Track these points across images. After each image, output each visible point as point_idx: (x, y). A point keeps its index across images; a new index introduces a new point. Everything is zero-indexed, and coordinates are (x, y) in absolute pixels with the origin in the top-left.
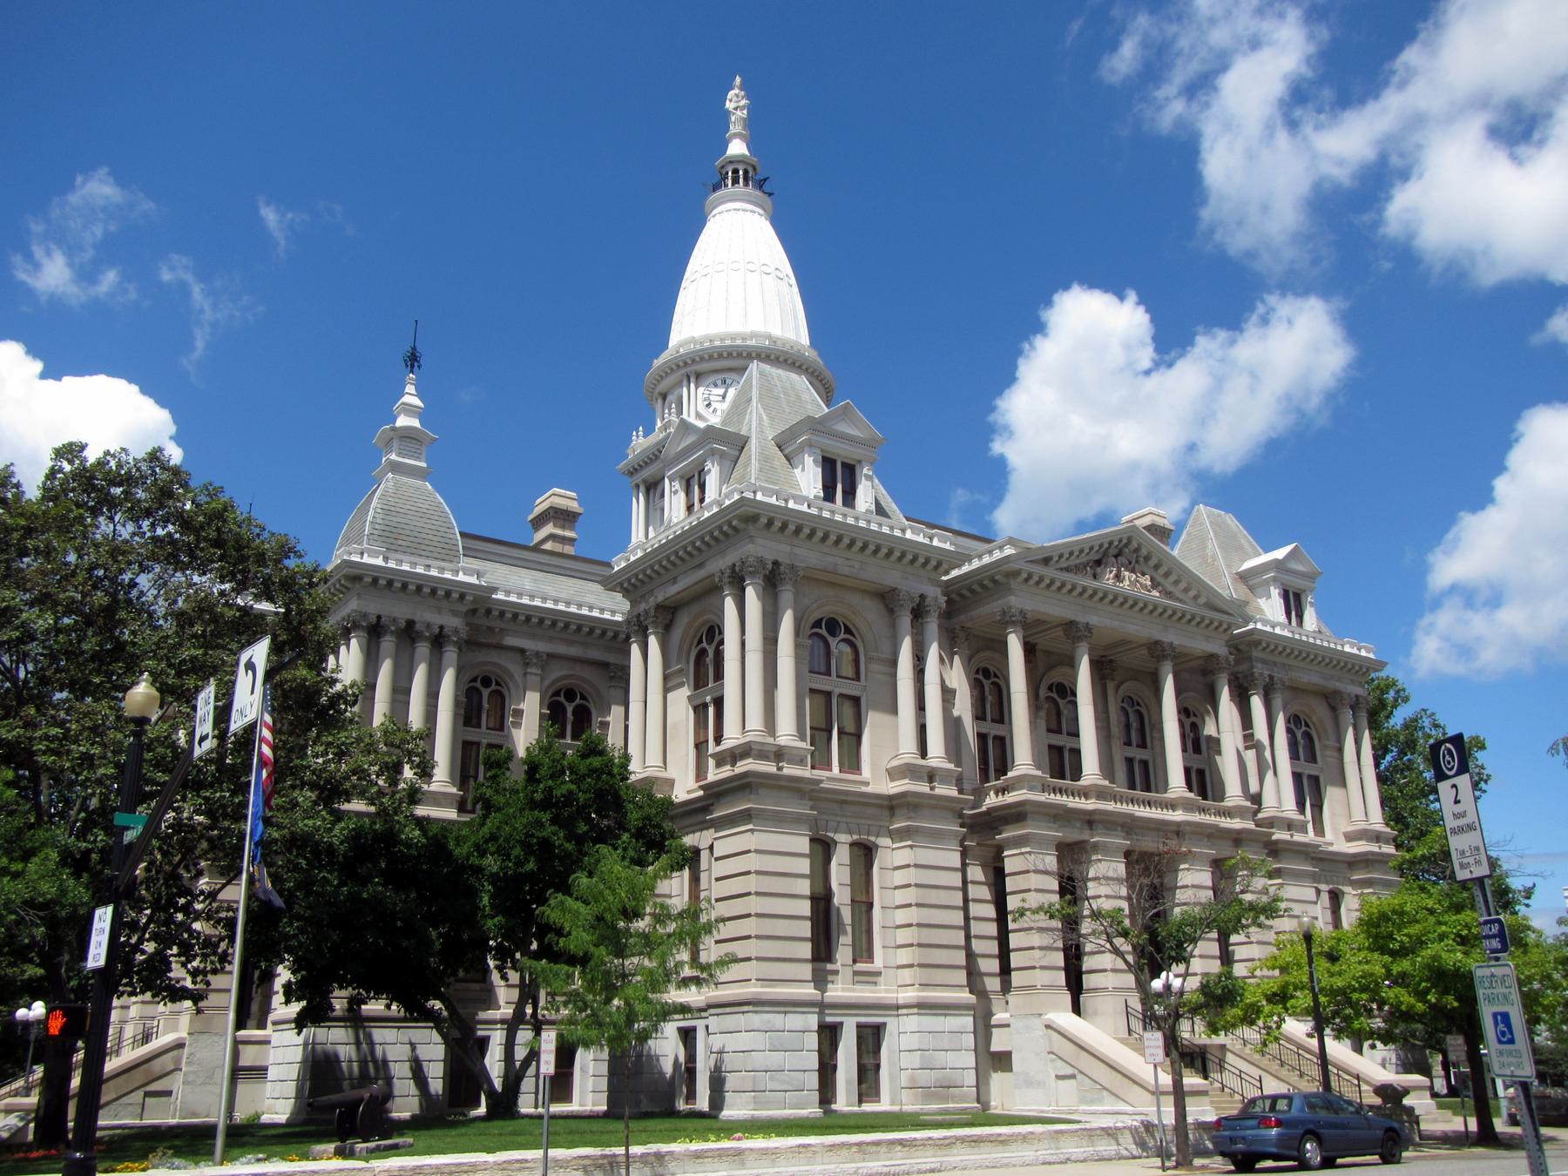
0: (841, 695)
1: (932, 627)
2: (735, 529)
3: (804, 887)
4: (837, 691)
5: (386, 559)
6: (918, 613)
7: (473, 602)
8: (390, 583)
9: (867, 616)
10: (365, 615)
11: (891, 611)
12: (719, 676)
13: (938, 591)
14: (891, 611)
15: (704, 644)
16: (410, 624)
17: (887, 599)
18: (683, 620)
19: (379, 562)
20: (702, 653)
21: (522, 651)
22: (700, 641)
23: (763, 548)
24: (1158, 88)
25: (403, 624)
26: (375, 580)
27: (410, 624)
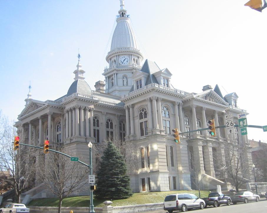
0: (167, 120)
6: (179, 106)
10: (78, 106)
20: (141, 113)
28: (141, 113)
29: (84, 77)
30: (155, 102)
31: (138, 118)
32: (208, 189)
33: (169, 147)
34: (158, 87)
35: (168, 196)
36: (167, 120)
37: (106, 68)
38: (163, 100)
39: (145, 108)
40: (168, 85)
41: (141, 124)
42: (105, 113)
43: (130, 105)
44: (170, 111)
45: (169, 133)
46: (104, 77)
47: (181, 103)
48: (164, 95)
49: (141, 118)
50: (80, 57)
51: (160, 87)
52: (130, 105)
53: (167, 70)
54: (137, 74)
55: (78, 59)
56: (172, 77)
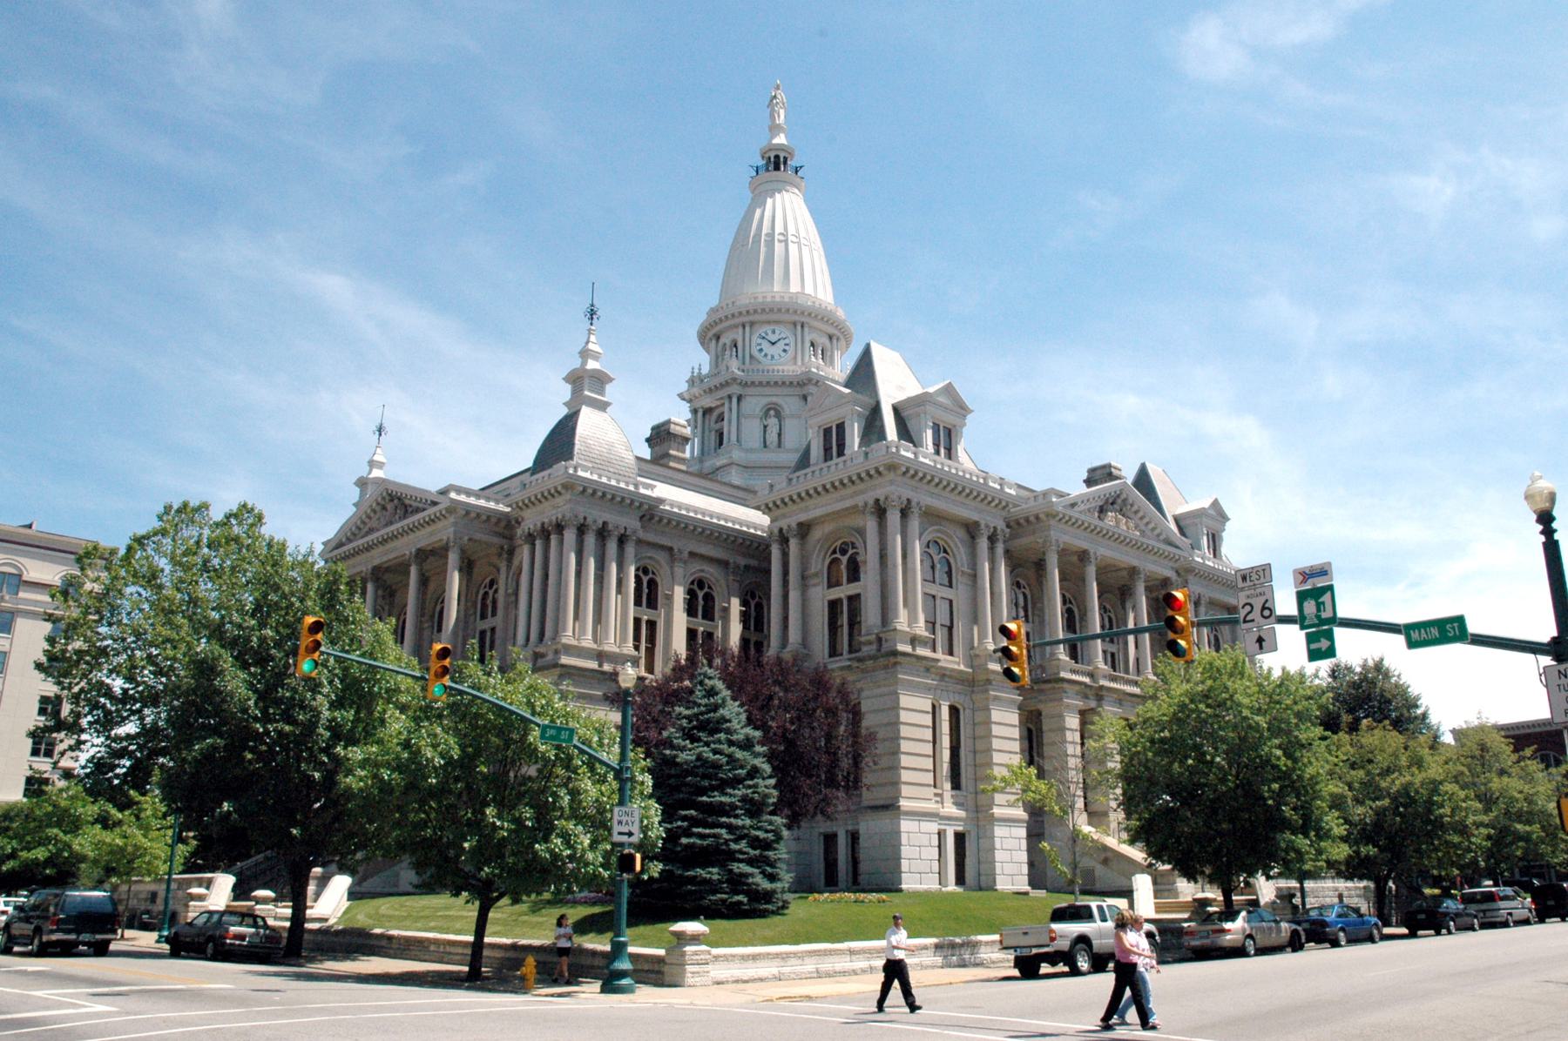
6: (992, 539)
11: (973, 537)
17: (971, 530)
21: (671, 549)
40: (950, 454)
42: (686, 555)
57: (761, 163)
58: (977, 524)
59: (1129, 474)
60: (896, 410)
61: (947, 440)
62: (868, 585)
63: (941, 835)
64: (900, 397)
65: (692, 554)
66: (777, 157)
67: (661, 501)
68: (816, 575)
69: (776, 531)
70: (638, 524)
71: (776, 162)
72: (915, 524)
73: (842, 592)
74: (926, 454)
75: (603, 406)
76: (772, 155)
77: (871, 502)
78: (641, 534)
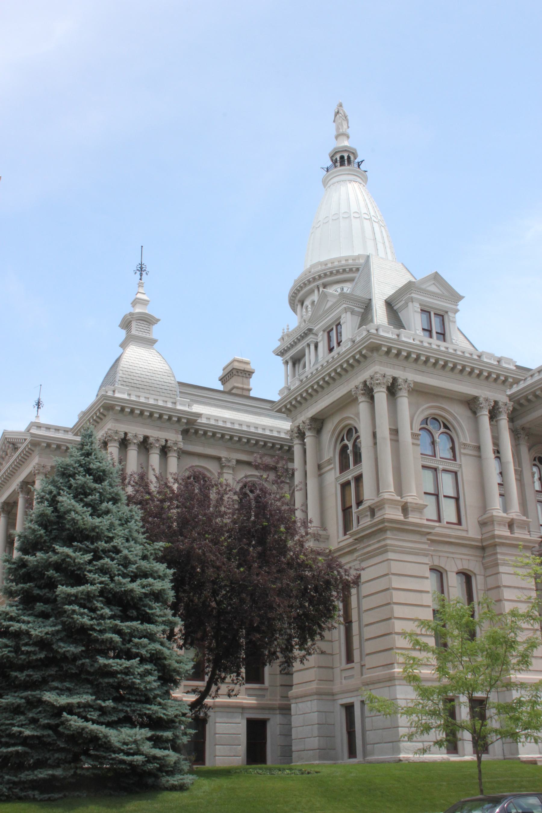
0: (444, 470)
1: (504, 423)
2: (365, 357)
3: (428, 599)
4: (441, 467)
5: (129, 395)
6: (493, 414)
7: (187, 423)
8: (59, 447)
9: (458, 415)
10: (116, 432)
11: (475, 413)
12: (358, 458)
13: (506, 400)
14: (475, 413)
15: (346, 442)
16: (146, 438)
17: (471, 404)
18: (329, 428)
19: (125, 396)
20: (344, 448)
21: (219, 459)
22: (343, 440)
23: (379, 370)
24: (194, 665)
25: (141, 438)
26: (123, 409)
27: (146, 438)
28: (344, 448)
29: (154, 336)
30: (381, 396)
31: (334, 468)
32: (216, 709)
33: (478, 577)
34: (395, 337)
35: (41, 768)
36: (444, 470)
37: (286, 331)
38: (419, 391)
39: (355, 428)
40: (442, 335)
41: (345, 486)
42: (234, 462)
43: (304, 423)
44: (458, 437)
45: (454, 520)
46: (280, 359)
47: (506, 404)
48: (424, 368)
49: (344, 467)
50: (144, 273)
51: (404, 339)
52: (304, 423)
53: (436, 277)
54: (330, 304)
55: (138, 281)
56: (461, 305)
57: (330, 163)
58: (475, 399)
59: (358, 160)
60: (389, 304)
61: (438, 320)
62: (366, 467)
63: (365, 754)
64: (389, 292)
65: (239, 462)
66: (342, 158)
67: (199, 415)
68: (329, 462)
69: (296, 430)
70: (180, 438)
71: (343, 159)
72: (404, 402)
73: (349, 476)
74: (413, 334)
75: (150, 343)
76: (338, 157)
77: (361, 386)
78: (181, 445)
